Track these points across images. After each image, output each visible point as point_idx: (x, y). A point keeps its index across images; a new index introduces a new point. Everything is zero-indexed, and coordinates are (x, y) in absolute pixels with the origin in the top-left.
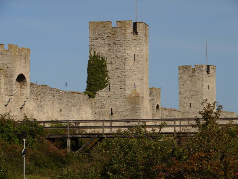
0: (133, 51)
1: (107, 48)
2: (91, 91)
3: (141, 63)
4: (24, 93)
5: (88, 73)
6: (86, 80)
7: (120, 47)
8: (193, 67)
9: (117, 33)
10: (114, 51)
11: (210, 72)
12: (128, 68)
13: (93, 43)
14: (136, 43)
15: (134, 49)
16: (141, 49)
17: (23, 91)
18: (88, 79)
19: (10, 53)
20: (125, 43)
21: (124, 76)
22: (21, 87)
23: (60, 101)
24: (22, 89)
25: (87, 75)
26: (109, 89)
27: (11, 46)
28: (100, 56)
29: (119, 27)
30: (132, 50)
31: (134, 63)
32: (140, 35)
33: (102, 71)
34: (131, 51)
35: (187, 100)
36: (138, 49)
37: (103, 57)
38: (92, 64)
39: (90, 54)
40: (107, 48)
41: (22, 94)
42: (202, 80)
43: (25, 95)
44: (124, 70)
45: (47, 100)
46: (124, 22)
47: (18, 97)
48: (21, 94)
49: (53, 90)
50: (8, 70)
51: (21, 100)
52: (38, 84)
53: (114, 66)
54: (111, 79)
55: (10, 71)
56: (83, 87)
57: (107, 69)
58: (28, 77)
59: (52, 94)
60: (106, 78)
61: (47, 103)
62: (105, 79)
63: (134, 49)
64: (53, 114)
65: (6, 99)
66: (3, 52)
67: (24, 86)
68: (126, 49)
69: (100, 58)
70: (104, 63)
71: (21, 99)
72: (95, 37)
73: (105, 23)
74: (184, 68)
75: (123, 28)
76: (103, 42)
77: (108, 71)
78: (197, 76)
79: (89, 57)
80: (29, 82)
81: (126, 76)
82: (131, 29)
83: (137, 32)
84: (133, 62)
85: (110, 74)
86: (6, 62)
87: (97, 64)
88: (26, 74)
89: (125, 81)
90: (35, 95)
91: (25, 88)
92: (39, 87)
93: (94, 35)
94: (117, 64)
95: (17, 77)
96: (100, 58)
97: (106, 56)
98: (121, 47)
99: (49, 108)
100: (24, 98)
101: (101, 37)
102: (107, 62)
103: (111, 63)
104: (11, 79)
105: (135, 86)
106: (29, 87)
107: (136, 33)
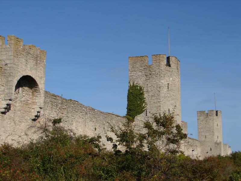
0: (167, 80)
1: (144, 78)
2: (130, 116)
3: (174, 91)
4: (36, 101)
5: (128, 100)
6: (126, 106)
7: (155, 77)
8: (207, 112)
9: (153, 65)
10: (150, 81)
11: (218, 115)
12: (162, 95)
13: (132, 74)
14: (169, 74)
15: (168, 79)
16: (174, 79)
18: (128, 106)
19: (9, 47)
20: (160, 74)
21: (159, 102)
22: (33, 95)
23: (94, 120)
24: (34, 97)
25: (127, 103)
26: (146, 114)
27: (11, 38)
28: (138, 86)
29: (155, 60)
30: (166, 80)
31: (168, 91)
32: (173, 67)
33: (140, 98)
34: (165, 81)
36: (171, 79)
37: (141, 86)
38: (132, 93)
39: (129, 85)
40: (144, 78)
41: (34, 103)
43: (38, 104)
44: (159, 97)
45: (76, 117)
46: (158, 55)
47: (30, 107)
48: (33, 102)
49: (86, 108)
50: (6, 68)
51: (33, 110)
52: (63, 97)
53: (151, 94)
55: (8, 69)
56: (124, 112)
57: (144, 97)
59: (84, 111)
62: (143, 105)
63: (167, 79)
64: (85, 131)
65: (3, 104)
67: (36, 94)
68: (161, 78)
69: (138, 87)
70: (142, 91)
71: (33, 109)
73: (142, 58)
74: (201, 113)
75: (158, 61)
76: (140, 74)
77: (145, 98)
78: (210, 117)
79: (129, 87)
80: (44, 89)
81: (161, 102)
82: (165, 62)
83: (170, 64)
84: (167, 91)
85: (147, 100)
87: (135, 92)
88: (38, 78)
89: (160, 106)
90: (58, 108)
91: (38, 96)
93: (133, 68)
96: (138, 87)
97: (143, 85)
98: (156, 77)
99: (79, 124)
100: (36, 108)
101: (139, 69)
102: (144, 91)
103: (148, 91)
104: (10, 79)
105: (169, 111)
106: (42, 95)
107: (170, 66)
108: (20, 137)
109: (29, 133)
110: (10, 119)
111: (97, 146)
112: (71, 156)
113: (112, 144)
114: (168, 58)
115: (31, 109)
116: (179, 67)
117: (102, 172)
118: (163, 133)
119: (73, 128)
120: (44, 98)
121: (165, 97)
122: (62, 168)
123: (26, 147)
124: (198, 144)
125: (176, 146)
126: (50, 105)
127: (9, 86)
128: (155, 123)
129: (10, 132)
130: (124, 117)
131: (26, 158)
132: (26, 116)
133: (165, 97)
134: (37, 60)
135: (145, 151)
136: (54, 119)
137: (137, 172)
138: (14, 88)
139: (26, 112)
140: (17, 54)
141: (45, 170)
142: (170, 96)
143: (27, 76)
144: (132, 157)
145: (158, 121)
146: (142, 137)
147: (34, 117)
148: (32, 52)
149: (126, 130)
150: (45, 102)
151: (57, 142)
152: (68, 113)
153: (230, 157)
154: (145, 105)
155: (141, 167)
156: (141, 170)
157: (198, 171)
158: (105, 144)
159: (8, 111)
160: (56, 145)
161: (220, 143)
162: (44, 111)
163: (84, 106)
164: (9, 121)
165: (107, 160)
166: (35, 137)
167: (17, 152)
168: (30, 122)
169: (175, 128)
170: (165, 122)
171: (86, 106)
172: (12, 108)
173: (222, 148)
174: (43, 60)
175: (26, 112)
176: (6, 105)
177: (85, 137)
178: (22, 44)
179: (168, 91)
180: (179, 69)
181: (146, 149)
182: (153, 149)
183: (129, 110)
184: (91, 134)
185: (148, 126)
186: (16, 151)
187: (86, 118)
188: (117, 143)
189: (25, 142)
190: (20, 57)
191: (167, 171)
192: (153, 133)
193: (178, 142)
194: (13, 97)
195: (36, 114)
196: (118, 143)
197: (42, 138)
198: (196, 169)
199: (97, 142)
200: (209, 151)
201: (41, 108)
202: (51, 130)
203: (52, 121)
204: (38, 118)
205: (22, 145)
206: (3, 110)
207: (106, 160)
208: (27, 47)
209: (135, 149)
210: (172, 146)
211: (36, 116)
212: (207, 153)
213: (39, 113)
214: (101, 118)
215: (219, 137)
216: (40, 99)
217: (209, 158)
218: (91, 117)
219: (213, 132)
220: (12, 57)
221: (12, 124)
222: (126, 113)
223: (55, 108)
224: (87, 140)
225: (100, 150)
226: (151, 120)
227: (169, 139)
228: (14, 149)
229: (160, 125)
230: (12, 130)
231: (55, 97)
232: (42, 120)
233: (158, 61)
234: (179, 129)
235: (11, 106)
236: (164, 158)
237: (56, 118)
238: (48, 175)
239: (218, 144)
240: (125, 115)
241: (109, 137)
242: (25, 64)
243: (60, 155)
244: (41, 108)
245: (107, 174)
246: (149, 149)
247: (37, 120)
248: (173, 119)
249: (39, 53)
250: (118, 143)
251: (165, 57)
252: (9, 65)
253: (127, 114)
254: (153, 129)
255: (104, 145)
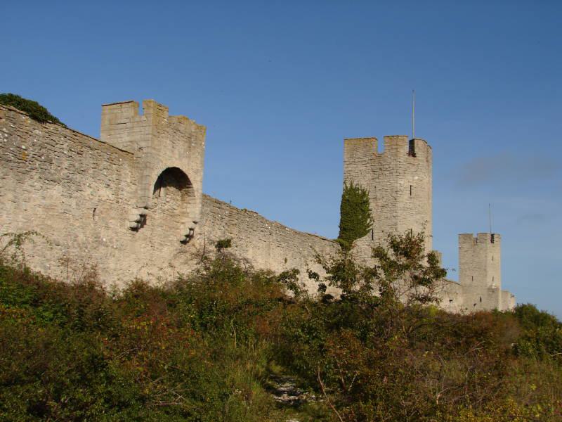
1: (369, 176)
8: (475, 236)
12: (400, 205)
13: (350, 169)
14: (413, 169)
15: (411, 178)
17: (186, 208)
22: (183, 200)
35: (468, 273)
36: (416, 178)
39: (344, 186)
40: (369, 176)
42: (486, 250)
43: (190, 216)
47: (177, 220)
48: (183, 213)
49: (270, 224)
51: (182, 226)
52: (234, 204)
53: (380, 203)
54: (376, 221)
56: (334, 233)
57: (370, 208)
58: (199, 179)
60: (368, 221)
61: (254, 242)
63: (410, 178)
65: (133, 215)
66: (133, 117)
71: (183, 223)
72: (352, 160)
73: (366, 141)
74: (466, 237)
75: (394, 147)
76: (364, 168)
77: (371, 210)
80: (200, 191)
82: (406, 148)
85: (374, 214)
86: (137, 137)
89: (396, 224)
90: (224, 224)
92: (235, 211)
94: (384, 200)
95: (163, 172)
99: (259, 252)
102: (370, 197)
103: (375, 198)
104: (146, 173)
106: (198, 201)
107: (414, 155)
108: (161, 269)
109: (176, 263)
110: (145, 239)
111: (293, 286)
112: (249, 303)
113: (318, 283)
114: (412, 143)
115: (179, 224)
116: (429, 158)
117: (300, 330)
118: (406, 267)
119: (249, 256)
120: (200, 206)
121: (404, 209)
122: (231, 323)
123: (171, 286)
124: (460, 291)
125: (427, 290)
126: (210, 218)
127: (143, 185)
128: (392, 250)
129: (145, 261)
130: (335, 241)
131: (172, 305)
132: (172, 235)
133: (404, 209)
134: (190, 143)
135: (376, 297)
136: (218, 240)
137: (359, 332)
138: (152, 188)
139: (171, 228)
140: (158, 131)
141: (204, 326)
142: (413, 204)
143: (174, 168)
144: (352, 306)
145: (397, 247)
146: (372, 273)
147: (184, 238)
148: (182, 128)
149: (342, 260)
150: (202, 213)
151: (223, 280)
152: (240, 232)
153: (513, 314)
154: (371, 221)
155: (367, 323)
156: (367, 328)
157: (462, 334)
158: (306, 283)
159: (142, 226)
160: (222, 284)
161: (497, 289)
162: (200, 228)
163: (266, 221)
164: (143, 242)
165: (309, 311)
166: (187, 269)
167: (157, 295)
168: (178, 245)
169: (426, 259)
170: (408, 248)
171: (270, 220)
172: (147, 222)
173: (500, 298)
174: (200, 142)
175: (171, 228)
176: (139, 217)
177: (269, 272)
178: (166, 114)
179: (411, 198)
180: (431, 161)
181: (376, 293)
182: (387, 293)
183: (343, 229)
184: (278, 269)
185: (379, 254)
186: (155, 292)
187: (269, 242)
188: (327, 283)
189: (170, 279)
190: (162, 137)
191: (412, 331)
192: (390, 267)
193: (430, 282)
194: (150, 204)
195: (187, 232)
196: (328, 282)
197: (198, 271)
198: (460, 330)
199: (293, 280)
200: (478, 303)
201: (195, 223)
202: (214, 259)
203: (216, 243)
204: (190, 239)
205: (163, 283)
206: (134, 225)
207: (307, 311)
208: (175, 121)
209: (358, 293)
210: (422, 290)
211: (187, 236)
212: (475, 305)
213: (192, 232)
214: (296, 241)
215: (494, 278)
216: (194, 208)
217: (477, 313)
218: (279, 240)
219: (485, 270)
220: (150, 136)
221: (148, 248)
222: (338, 235)
223: (219, 222)
224: (271, 278)
225: (297, 293)
226: (385, 246)
227: (416, 278)
228: (152, 289)
229: (401, 254)
230: (149, 258)
231: (218, 205)
232: (198, 242)
233: (394, 147)
234: (433, 260)
235: (147, 217)
236: (407, 309)
237: (223, 239)
238: (209, 333)
239: (493, 291)
240: (336, 238)
241: (313, 272)
242: (170, 147)
243: (229, 301)
244: (195, 223)
245: (308, 333)
246: (381, 294)
247: (188, 242)
248: (422, 243)
249: (193, 130)
250: (328, 282)
251: (407, 140)
252: (144, 149)
253: (339, 237)
254: (389, 259)
255: (304, 285)
